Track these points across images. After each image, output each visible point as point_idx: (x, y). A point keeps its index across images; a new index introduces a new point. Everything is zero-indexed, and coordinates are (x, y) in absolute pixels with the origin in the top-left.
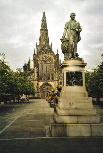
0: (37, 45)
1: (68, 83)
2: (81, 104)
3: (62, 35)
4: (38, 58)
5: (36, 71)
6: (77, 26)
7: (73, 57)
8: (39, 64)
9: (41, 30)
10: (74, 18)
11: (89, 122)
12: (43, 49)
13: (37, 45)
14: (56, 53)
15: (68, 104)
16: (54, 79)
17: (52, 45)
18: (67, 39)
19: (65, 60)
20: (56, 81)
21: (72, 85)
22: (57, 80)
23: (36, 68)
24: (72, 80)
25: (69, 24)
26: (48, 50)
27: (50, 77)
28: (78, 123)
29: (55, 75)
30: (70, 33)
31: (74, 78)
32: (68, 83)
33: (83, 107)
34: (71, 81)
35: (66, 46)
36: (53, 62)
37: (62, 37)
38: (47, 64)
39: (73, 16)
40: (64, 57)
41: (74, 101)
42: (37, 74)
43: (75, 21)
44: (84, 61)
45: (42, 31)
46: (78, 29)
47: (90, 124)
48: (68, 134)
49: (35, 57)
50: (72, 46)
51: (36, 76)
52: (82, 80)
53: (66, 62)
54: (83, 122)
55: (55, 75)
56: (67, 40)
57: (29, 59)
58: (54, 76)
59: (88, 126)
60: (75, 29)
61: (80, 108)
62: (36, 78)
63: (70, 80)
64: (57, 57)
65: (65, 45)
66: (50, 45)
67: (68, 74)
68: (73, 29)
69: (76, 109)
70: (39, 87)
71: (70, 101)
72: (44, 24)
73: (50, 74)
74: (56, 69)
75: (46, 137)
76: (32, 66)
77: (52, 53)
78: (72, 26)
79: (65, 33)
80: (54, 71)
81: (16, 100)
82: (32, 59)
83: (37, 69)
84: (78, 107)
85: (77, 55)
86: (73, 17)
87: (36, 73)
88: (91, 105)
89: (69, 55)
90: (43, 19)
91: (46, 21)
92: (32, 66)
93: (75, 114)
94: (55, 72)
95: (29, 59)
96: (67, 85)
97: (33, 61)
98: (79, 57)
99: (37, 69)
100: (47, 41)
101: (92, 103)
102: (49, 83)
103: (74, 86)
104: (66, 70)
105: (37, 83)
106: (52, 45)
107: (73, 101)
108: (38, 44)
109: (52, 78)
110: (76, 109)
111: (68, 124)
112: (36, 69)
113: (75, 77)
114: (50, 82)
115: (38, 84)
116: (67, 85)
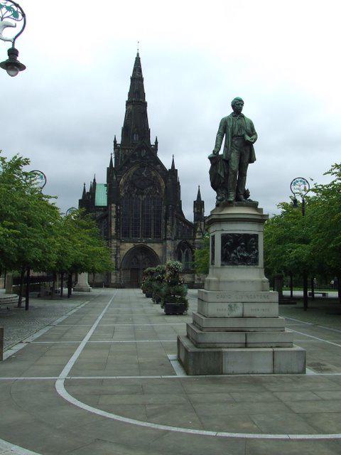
0: (115, 142)
1: (226, 259)
2: (253, 306)
3: (213, 148)
4: (121, 177)
5: (114, 214)
6: (248, 128)
7: (237, 199)
8: (122, 194)
9: (128, 103)
10: (241, 109)
11: (269, 345)
12: (133, 156)
13: (115, 142)
14: (168, 167)
15: (226, 306)
16: (163, 236)
17: (156, 143)
18: (224, 157)
19: (217, 205)
20: (167, 242)
21: (236, 264)
22: (169, 239)
23: (113, 205)
24: (236, 254)
25: (230, 124)
26: (148, 157)
27: (152, 230)
28: (246, 347)
29: (166, 224)
30: (232, 142)
31: (239, 248)
32: (226, 259)
33: (258, 314)
34: (233, 255)
35: (222, 174)
36: (160, 189)
37: (214, 151)
38: (145, 197)
39: (239, 104)
40: (217, 198)
41: (239, 300)
42: (117, 222)
43: (243, 116)
44: (262, 209)
45: (131, 107)
46: (250, 136)
47: (271, 347)
48: (223, 369)
49: (113, 176)
50: (235, 173)
51: (113, 228)
52: (257, 253)
53: (222, 210)
54: (230, 345)
55: (166, 227)
56: (224, 160)
57: (94, 180)
58: (163, 226)
59: (267, 352)
60: (243, 136)
61: (252, 316)
62: (113, 232)
63: (231, 251)
64: (171, 178)
65: (219, 171)
66: (153, 142)
67: (225, 238)
68: (239, 134)
69: (243, 317)
70: (122, 257)
71: (229, 300)
72: (136, 88)
73: (153, 221)
74: (167, 208)
75: (175, 374)
76: (101, 199)
77: (158, 166)
78: (237, 129)
79: (219, 143)
80: (163, 215)
81: (67, 289)
82: (102, 179)
83: (117, 209)
84: (247, 313)
85: (247, 194)
86: (237, 105)
87: (114, 220)
88: (275, 309)
89: (227, 195)
90: (134, 74)
91: (141, 79)
92: (101, 199)
93: (239, 329)
94: (166, 218)
95: (94, 180)
96: (222, 265)
97: (106, 185)
98: (249, 198)
99: (116, 207)
100: (146, 132)
101: (277, 306)
102: (149, 245)
103: (239, 266)
104: (223, 230)
105: (117, 247)
106: (156, 143)
107: (236, 300)
108: (119, 142)
109: (158, 234)
110: (243, 317)
111: (226, 350)
112: (114, 209)
113: (242, 246)
114: (152, 244)
115: (118, 249)
116: (224, 263)
